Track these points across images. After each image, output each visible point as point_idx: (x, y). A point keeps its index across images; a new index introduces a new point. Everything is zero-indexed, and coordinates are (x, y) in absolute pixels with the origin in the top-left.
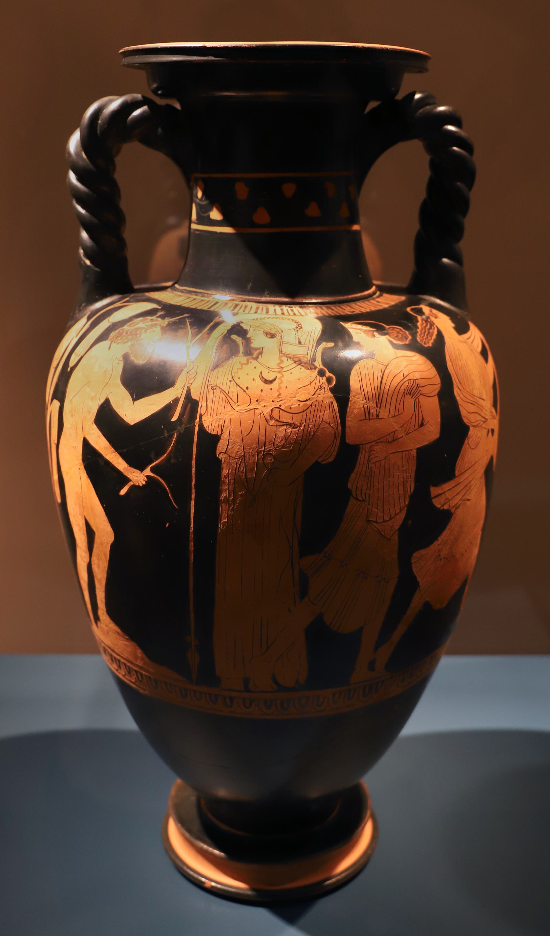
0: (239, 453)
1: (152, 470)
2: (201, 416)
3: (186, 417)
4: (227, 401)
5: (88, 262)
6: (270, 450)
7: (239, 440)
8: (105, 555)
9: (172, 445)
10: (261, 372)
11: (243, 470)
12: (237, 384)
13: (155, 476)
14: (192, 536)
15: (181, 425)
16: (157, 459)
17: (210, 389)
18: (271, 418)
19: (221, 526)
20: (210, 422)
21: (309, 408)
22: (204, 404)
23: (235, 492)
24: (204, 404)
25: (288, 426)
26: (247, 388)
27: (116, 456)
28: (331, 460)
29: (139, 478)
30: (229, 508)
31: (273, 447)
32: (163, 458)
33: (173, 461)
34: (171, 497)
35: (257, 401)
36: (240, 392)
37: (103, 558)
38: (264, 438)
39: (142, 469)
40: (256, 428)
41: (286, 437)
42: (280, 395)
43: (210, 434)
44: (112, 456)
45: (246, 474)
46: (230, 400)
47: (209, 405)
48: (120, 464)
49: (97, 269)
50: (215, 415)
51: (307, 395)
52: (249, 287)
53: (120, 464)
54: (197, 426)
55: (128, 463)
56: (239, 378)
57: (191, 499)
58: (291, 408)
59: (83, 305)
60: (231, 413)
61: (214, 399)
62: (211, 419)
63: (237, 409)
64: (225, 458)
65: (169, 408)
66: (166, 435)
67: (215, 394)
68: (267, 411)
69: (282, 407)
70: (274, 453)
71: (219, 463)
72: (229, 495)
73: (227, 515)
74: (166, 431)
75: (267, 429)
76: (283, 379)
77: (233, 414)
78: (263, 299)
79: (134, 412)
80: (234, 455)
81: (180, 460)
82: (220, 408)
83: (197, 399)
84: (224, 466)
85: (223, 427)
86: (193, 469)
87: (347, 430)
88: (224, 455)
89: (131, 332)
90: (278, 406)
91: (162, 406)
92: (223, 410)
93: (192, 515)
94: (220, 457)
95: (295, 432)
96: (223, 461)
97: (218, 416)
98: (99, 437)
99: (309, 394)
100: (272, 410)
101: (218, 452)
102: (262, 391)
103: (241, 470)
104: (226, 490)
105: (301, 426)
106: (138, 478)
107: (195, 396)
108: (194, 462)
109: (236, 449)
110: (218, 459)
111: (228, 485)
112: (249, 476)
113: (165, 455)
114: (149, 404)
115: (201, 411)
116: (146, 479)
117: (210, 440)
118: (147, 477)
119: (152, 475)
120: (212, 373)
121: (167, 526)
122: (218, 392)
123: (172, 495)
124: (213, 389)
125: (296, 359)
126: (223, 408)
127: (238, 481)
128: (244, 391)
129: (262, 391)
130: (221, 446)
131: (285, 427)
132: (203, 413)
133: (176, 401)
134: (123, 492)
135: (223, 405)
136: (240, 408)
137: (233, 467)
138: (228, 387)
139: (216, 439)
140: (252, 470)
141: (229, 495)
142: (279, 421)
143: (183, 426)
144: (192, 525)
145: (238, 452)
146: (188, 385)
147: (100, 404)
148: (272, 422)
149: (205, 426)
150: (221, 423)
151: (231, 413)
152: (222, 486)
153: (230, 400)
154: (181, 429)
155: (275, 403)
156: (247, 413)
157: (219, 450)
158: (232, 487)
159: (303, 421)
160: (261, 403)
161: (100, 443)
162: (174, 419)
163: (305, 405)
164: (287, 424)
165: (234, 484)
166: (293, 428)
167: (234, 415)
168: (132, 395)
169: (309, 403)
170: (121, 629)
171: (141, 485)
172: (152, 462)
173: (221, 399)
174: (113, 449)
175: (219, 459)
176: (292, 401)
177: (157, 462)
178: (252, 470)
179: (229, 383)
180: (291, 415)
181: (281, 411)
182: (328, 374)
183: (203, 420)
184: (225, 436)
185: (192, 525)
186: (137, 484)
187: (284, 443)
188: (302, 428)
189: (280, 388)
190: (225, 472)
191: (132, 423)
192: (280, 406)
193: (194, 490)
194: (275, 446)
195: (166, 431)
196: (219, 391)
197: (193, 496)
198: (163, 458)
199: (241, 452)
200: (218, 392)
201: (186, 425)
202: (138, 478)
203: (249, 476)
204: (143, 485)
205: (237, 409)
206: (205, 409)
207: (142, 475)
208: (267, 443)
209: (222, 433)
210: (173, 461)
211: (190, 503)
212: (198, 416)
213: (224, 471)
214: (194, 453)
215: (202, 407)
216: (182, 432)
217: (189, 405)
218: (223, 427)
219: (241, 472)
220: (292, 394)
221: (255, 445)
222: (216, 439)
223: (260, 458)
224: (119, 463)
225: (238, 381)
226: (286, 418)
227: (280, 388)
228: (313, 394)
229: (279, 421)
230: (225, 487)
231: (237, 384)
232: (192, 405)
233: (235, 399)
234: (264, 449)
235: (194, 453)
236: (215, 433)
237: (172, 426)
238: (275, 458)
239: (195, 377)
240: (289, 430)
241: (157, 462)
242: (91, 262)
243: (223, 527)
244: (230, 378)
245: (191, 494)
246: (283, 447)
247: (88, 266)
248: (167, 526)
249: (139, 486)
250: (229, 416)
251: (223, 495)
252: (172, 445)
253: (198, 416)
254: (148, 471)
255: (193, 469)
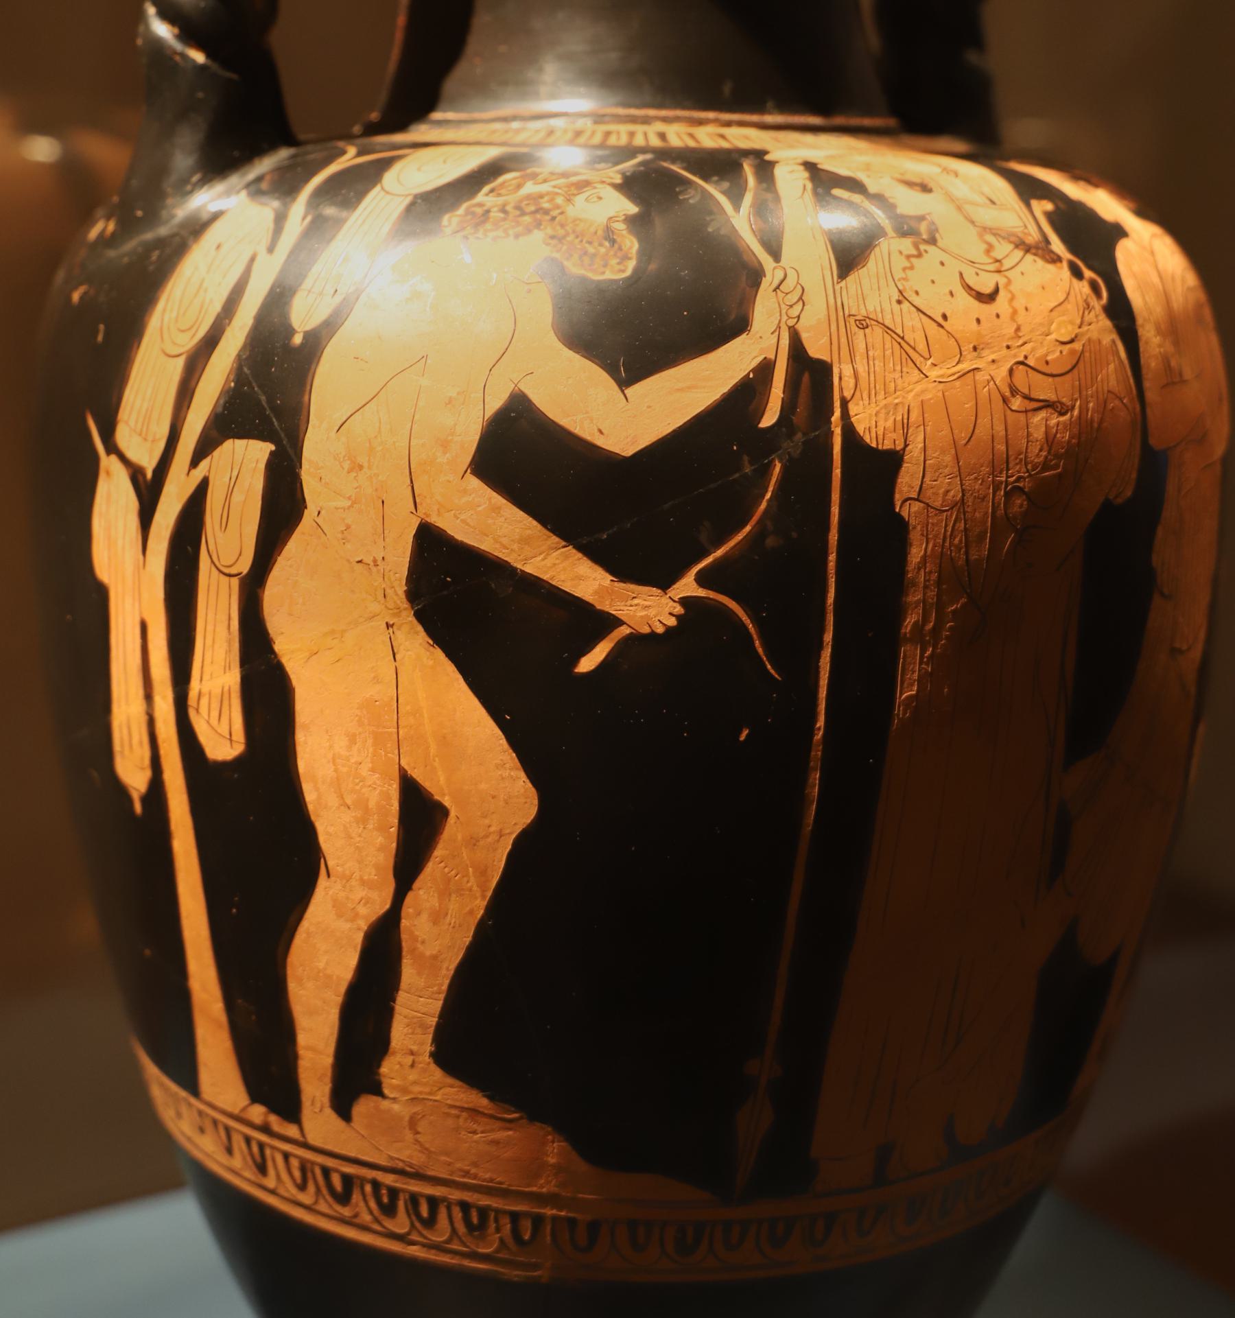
0: (952, 493)
1: (702, 580)
2: (845, 403)
3: (802, 410)
4: (904, 356)
5: (199, 57)
6: (1018, 480)
7: (948, 458)
8: (483, 872)
9: (768, 496)
10: (961, 274)
11: (961, 541)
12: (919, 310)
13: (712, 595)
14: (817, 753)
15: (791, 434)
16: (718, 547)
17: (855, 329)
18: (1014, 391)
19: (899, 710)
20: (872, 420)
21: (1080, 362)
22: (847, 371)
23: (940, 606)
24: (847, 371)
25: (1050, 410)
26: (945, 317)
27: (567, 557)
28: (1129, 493)
29: (652, 612)
30: (923, 651)
31: (1024, 469)
32: (740, 537)
33: (770, 542)
34: (760, 650)
35: (975, 349)
36: (932, 328)
37: (473, 882)
38: (1003, 448)
39: (664, 584)
40: (984, 421)
41: (1050, 440)
42: (1018, 329)
43: (875, 451)
44: (549, 562)
45: (967, 553)
46: (911, 352)
47: (862, 369)
48: (584, 579)
49: (228, 74)
50: (881, 395)
51: (1070, 328)
52: (727, 89)
53: (584, 579)
54: (838, 431)
55: (612, 573)
56: (917, 293)
57: (820, 646)
58: (1047, 363)
59: (195, 178)
60: (919, 388)
61: (871, 353)
62: (873, 409)
63: (934, 374)
64: (918, 514)
65: (749, 391)
66: (748, 469)
67: (870, 340)
68: (1001, 373)
69: (1031, 362)
70: (1026, 485)
71: (900, 527)
72: (925, 619)
73: (916, 676)
74: (746, 458)
75: (1009, 422)
76: (1012, 288)
77: (923, 392)
78: (769, 119)
79: (628, 417)
80: (938, 504)
81: (794, 535)
82: (890, 376)
83: (825, 357)
84: (915, 536)
85: (906, 426)
86: (832, 558)
87: (1149, 411)
88: (916, 506)
89: (517, 208)
90: (1021, 359)
91: (725, 389)
92: (899, 382)
93: (823, 693)
94: (905, 514)
95: (1064, 423)
96: (912, 522)
97: (889, 399)
98: (496, 509)
99: (1072, 322)
100: (1011, 371)
101: (898, 498)
102: (978, 321)
103: (957, 541)
104: (917, 603)
105: (1073, 407)
106: (649, 609)
107: (816, 349)
108: (834, 536)
109: (944, 487)
110: (899, 517)
111: (926, 587)
112: (973, 557)
113: (748, 528)
114: (678, 390)
115: (841, 389)
116: (679, 609)
117: (875, 468)
118: (684, 602)
119: (701, 593)
120: (843, 284)
121: (743, 737)
122: (876, 334)
123: (763, 645)
124: (863, 325)
125: (1013, 239)
126: (897, 375)
127: (952, 575)
128: (942, 326)
129: (978, 321)
130: (907, 482)
131: (1043, 414)
132: (847, 394)
133: (765, 369)
134: (587, 664)
135: (898, 368)
136: (941, 372)
137: (936, 536)
138: (898, 320)
139: (892, 461)
140: (981, 537)
141: (925, 619)
142: (1031, 399)
143: (799, 437)
144: (821, 722)
145: (948, 492)
146: (791, 322)
147: (489, 413)
148: (1017, 403)
149: (860, 429)
150: (899, 418)
151: (919, 388)
152: (907, 595)
153: (911, 352)
154: (794, 445)
155: (1013, 352)
156: (958, 383)
157: (901, 492)
158: (932, 593)
159: (1076, 396)
160: (985, 353)
161: (496, 527)
162: (769, 419)
163: (1072, 352)
164: (1047, 405)
165: (939, 582)
166: (1062, 414)
167: (932, 392)
168: (612, 370)
169: (1077, 346)
170: (491, 1098)
171: (660, 630)
172: (705, 554)
173: (888, 352)
174: (555, 539)
175: (902, 518)
176: (1045, 343)
177: (719, 553)
178: (981, 537)
179: (896, 307)
180: (1050, 379)
181: (1030, 371)
182: (1088, 273)
183: (852, 413)
184: (914, 452)
185: (821, 722)
186: (646, 630)
187: (1046, 457)
188: (1076, 412)
189: (1015, 312)
190: (916, 553)
191: (629, 451)
192: (1026, 357)
193: (830, 618)
194: (1029, 467)
195: (746, 458)
196: (878, 330)
197: (828, 637)
198: (740, 537)
199: (955, 494)
200: (876, 334)
201: (804, 434)
202: (649, 609)
203: (973, 557)
204: (669, 630)
205: (934, 374)
206: (852, 381)
207: (665, 600)
208: (1012, 459)
209: (906, 445)
210: (770, 542)
211: (819, 657)
212: (837, 404)
213: (914, 550)
214: (835, 510)
215: (844, 378)
216: (796, 453)
217: (806, 378)
218: (906, 426)
219: (956, 546)
220: (1041, 324)
221: (986, 470)
222: (892, 461)
223: (999, 504)
224: (580, 578)
225: (917, 301)
226: (1045, 390)
227: (1015, 312)
228: (1078, 321)
229: (1031, 399)
230: (914, 597)
231: (919, 310)
232: (810, 375)
233: (921, 346)
234: (1008, 477)
235: (835, 510)
236: (887, 445)
237: (768, 442)
238: (1029, 499)
239: (801, 298)
240: (1053, 422)
241: (719, 553)
242: (209, 55)
243: (904, 714)
244: (896, 296)
245: (822, 630)
246: (1046, 466)
247: (202, 68)
248: (743, 737)
249: (653, 634)
250: (917, 395)
251: (910, 620)
252: (768, 496)
253: (837, 404)
254: (687, 586)
255: (832, 558)
